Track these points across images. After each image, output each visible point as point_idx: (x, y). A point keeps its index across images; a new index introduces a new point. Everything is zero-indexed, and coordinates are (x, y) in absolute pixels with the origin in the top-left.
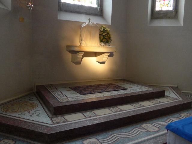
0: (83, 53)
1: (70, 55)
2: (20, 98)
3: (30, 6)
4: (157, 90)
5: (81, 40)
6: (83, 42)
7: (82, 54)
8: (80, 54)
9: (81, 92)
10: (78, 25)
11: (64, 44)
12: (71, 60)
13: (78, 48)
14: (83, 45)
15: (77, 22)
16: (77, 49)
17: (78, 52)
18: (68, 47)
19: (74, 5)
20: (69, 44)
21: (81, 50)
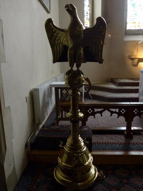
0: (88, 84)
1: (130, 61)
2: (14, 158)
3: (109, 37)
4: (49, 10)
5: (138, 51)
6: (138, 53)
7: (137, 60)
8: (136, 60)
9: (133, 80)
10: (136, 43)
11: (127, 55)
12: (131, 64)
13: (134, 56)
14: (138, 55)
15: (136, 41)
16: (133, 57)
17: (134, 59)
18: (129, 56)
19: (135, 30)
20: (130, 54)
21: (136, 58)
